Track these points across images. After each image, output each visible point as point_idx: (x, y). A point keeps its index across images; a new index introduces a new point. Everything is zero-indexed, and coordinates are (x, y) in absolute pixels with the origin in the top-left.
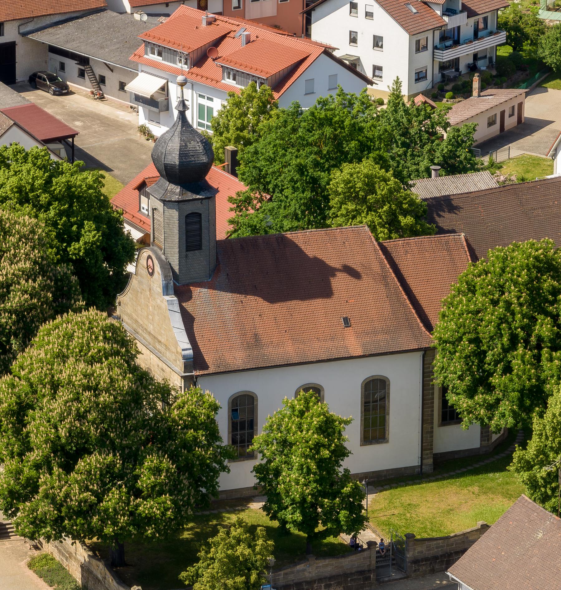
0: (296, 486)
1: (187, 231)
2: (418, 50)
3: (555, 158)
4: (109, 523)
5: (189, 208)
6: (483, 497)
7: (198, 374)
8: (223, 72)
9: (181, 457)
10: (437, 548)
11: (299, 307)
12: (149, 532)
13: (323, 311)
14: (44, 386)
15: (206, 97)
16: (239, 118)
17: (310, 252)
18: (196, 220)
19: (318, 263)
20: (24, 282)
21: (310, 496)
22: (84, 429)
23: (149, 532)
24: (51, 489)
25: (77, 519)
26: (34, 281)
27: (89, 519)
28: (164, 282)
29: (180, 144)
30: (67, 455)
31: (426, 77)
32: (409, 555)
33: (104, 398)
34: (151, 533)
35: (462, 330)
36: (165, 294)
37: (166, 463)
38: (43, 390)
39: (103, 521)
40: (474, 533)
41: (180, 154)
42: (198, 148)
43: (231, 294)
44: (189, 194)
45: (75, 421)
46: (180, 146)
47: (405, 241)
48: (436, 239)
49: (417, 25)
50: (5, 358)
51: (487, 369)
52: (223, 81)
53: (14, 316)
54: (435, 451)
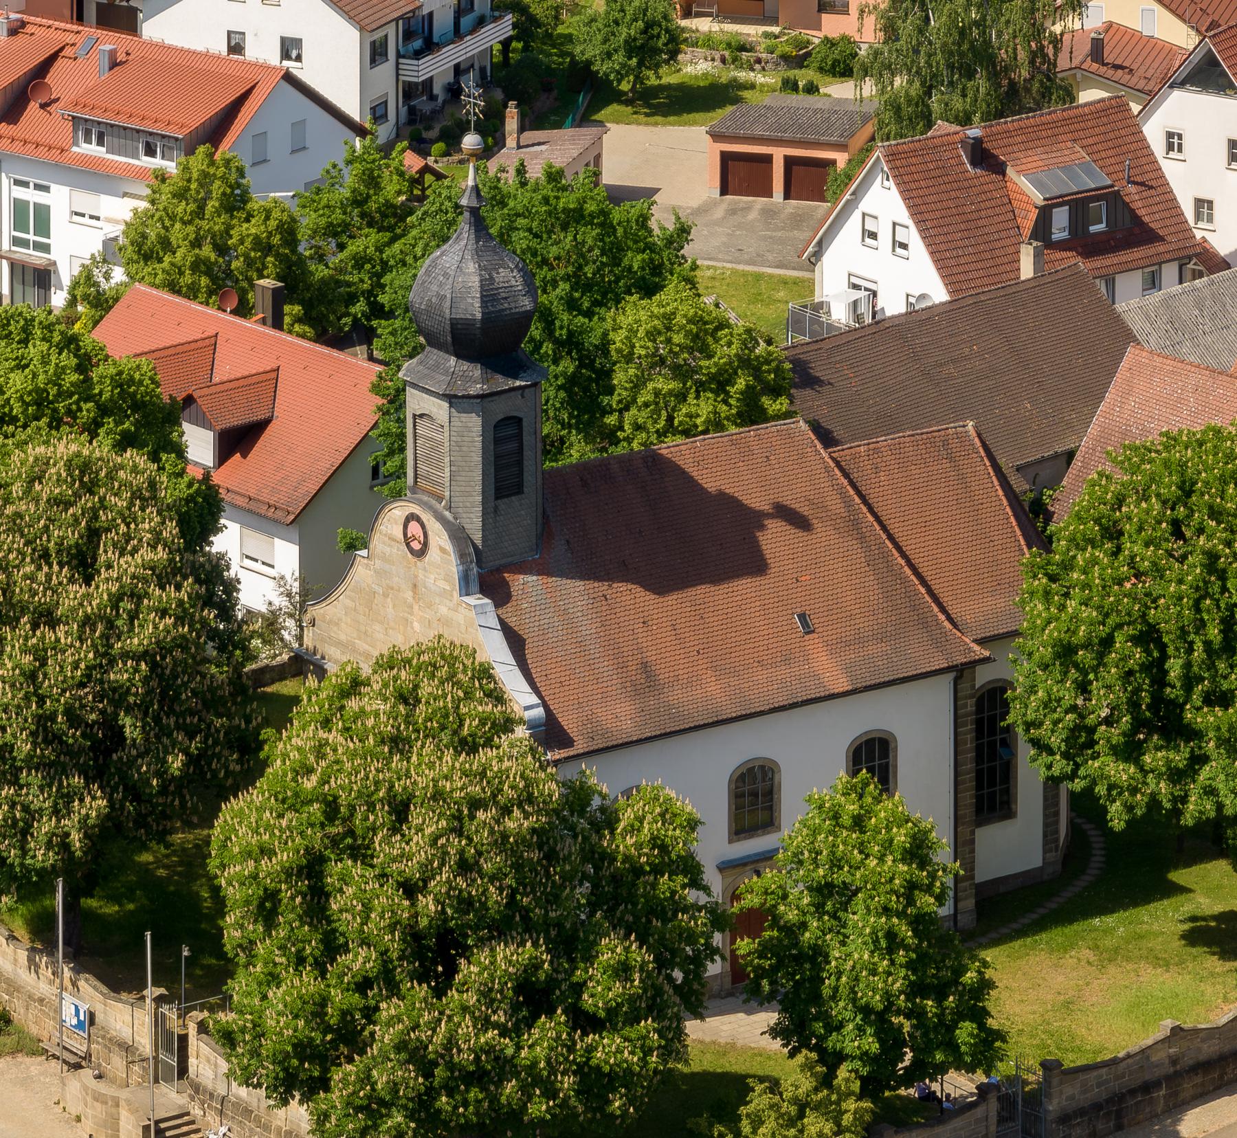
0: (871, 978)
1: (497, 457)
2: (373, 61)
3: (819, 260)
4: (538, 1092)
5: (501, 409)
6: (1112, 969)
7: (558, 757)
8: (75, 131)
9: (652, 935)
10: (1099, 1085)
11: (711, 599)
12: (617, 1104)
13: (758, 603)
14: (371, 807)
15: (32, 185)
16: (190, 222)
17: (711, 482)
18: (511, 431)
19: (727, 502)
20: (158, 592)
21: (902, 997)
22: (474, 893)
23: (617, 1104)
24: (413, 1029)
25: (467, 1091)
26: (178, 588)
27: (492, 1088)
28: (461, 568)
29: (481, 275)
30: (435, 954)
31: (386, 115)
32: (1053, 1106)
33: (515, 823)
34: (619, 1108)
35: (1111, 621)
36: (464, 592)
37: (640, 955)
38: (372, 818)
39: (525, 1089)
40: (1160, 1046)
41: (482, 296)
42: (514, 283)
43: (582, 583)
44: (500, 378)
45: (455, 877)
46: (481, 281)
47: (871, 446)
48: (924, 436)
49: (370, 12)
50: (121, 758)
51: (1172, 696)
52: (75, 149)
53: (143, 666)
54: (977, 880)
